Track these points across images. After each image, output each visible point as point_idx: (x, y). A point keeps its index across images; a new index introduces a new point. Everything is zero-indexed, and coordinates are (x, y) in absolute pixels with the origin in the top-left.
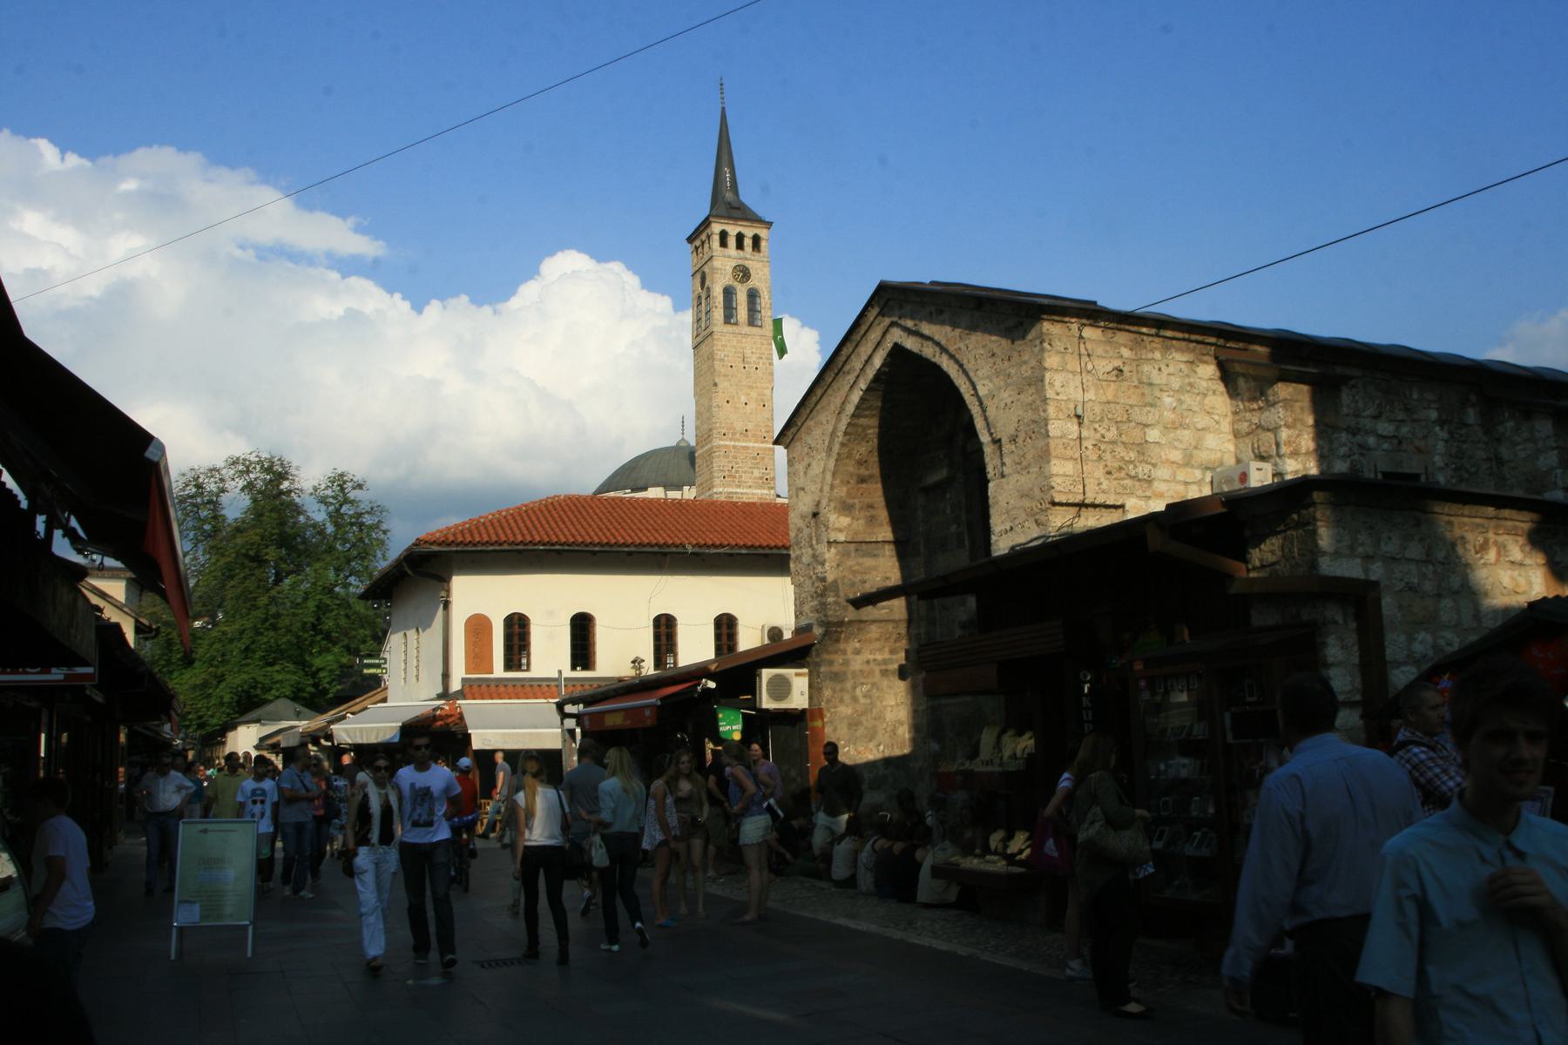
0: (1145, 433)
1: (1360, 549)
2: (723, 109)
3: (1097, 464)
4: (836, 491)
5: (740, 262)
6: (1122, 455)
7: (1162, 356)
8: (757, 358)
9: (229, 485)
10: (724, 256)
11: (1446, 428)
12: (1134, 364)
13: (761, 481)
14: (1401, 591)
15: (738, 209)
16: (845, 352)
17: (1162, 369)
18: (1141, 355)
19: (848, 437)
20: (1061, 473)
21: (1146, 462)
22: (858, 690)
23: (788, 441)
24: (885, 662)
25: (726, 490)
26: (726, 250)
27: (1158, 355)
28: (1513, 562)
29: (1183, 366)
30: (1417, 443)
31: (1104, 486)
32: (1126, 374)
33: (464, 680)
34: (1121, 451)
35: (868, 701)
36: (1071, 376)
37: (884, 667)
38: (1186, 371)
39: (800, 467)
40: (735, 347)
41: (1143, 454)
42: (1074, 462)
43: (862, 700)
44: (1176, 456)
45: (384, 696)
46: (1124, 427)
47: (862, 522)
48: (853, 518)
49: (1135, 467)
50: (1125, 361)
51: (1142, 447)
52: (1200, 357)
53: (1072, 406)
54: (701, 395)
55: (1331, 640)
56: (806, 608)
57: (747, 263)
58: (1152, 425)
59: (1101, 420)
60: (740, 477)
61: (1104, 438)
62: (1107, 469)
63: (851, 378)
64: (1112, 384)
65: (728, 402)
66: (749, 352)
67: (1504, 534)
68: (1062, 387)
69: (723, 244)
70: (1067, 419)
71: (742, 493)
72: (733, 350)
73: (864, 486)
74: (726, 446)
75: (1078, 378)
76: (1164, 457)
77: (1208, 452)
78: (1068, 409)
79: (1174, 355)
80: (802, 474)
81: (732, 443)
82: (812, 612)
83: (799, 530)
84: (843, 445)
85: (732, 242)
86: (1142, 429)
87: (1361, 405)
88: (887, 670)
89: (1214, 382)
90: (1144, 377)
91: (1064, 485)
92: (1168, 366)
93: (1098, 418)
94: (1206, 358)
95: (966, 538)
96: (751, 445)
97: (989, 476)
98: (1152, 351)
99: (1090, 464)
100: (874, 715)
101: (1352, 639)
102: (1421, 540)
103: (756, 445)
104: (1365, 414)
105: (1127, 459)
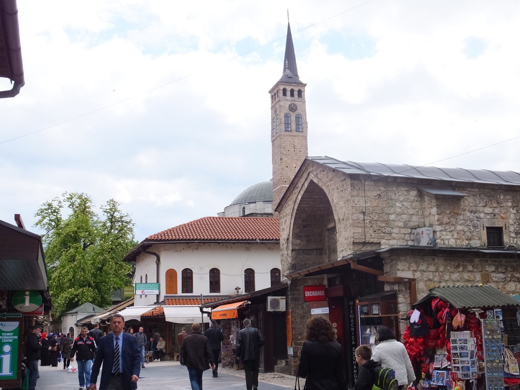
0: (389, 217)
1: (412, 268)
3: (370, 228)
5: (292, 102)
6: (380, 225)
7: (396, 189)
8: (300, 146)
9: (63, 204)
10: (285, 100)
11: (515, 209)
12: (385, 193)
14: (426, 281)
16: (296, 180)
21: (389, 227)
22: (304, 305)
26: (286, 97)
27: (395, 189)
28: (469, 271)
29: (405, 192)
30: (502, 215)
32: (382, 196)
33: (165, 297)
34: (379, 223)
36: (361, 198)
38: (406, 194)
40: (290, 142)
41: (388, 224)
43: (306, 308)
44: (401, 224)
45: (133, 302)
46: (381, 215)
48: (301, 240)
49: (385, 229)
50: (382, 191)
51: (387, 222)
52: (411, 188)
53: (361, 208)
54: (275, 163)
55: (400, 296)
57: (296, 103)
59: (372, 213)
61: (373, 219)
65: (287, 167)
66: (296, 143)
67: (466, 262)
69: (285, 94)
72: (289, 143)
73: (305, 228)
75: (364, 199)
78: (360, 210)
79: (401, 188)
80: (284, 223)
84: (296, 214)
85: (288, 93)
86: (388, 215)
87: (478, 202)
98: (393, 187)
99: (368, 228)
101: (407, 296)
102: (434, 265)
104: (479, 205)
105: (382, 226)
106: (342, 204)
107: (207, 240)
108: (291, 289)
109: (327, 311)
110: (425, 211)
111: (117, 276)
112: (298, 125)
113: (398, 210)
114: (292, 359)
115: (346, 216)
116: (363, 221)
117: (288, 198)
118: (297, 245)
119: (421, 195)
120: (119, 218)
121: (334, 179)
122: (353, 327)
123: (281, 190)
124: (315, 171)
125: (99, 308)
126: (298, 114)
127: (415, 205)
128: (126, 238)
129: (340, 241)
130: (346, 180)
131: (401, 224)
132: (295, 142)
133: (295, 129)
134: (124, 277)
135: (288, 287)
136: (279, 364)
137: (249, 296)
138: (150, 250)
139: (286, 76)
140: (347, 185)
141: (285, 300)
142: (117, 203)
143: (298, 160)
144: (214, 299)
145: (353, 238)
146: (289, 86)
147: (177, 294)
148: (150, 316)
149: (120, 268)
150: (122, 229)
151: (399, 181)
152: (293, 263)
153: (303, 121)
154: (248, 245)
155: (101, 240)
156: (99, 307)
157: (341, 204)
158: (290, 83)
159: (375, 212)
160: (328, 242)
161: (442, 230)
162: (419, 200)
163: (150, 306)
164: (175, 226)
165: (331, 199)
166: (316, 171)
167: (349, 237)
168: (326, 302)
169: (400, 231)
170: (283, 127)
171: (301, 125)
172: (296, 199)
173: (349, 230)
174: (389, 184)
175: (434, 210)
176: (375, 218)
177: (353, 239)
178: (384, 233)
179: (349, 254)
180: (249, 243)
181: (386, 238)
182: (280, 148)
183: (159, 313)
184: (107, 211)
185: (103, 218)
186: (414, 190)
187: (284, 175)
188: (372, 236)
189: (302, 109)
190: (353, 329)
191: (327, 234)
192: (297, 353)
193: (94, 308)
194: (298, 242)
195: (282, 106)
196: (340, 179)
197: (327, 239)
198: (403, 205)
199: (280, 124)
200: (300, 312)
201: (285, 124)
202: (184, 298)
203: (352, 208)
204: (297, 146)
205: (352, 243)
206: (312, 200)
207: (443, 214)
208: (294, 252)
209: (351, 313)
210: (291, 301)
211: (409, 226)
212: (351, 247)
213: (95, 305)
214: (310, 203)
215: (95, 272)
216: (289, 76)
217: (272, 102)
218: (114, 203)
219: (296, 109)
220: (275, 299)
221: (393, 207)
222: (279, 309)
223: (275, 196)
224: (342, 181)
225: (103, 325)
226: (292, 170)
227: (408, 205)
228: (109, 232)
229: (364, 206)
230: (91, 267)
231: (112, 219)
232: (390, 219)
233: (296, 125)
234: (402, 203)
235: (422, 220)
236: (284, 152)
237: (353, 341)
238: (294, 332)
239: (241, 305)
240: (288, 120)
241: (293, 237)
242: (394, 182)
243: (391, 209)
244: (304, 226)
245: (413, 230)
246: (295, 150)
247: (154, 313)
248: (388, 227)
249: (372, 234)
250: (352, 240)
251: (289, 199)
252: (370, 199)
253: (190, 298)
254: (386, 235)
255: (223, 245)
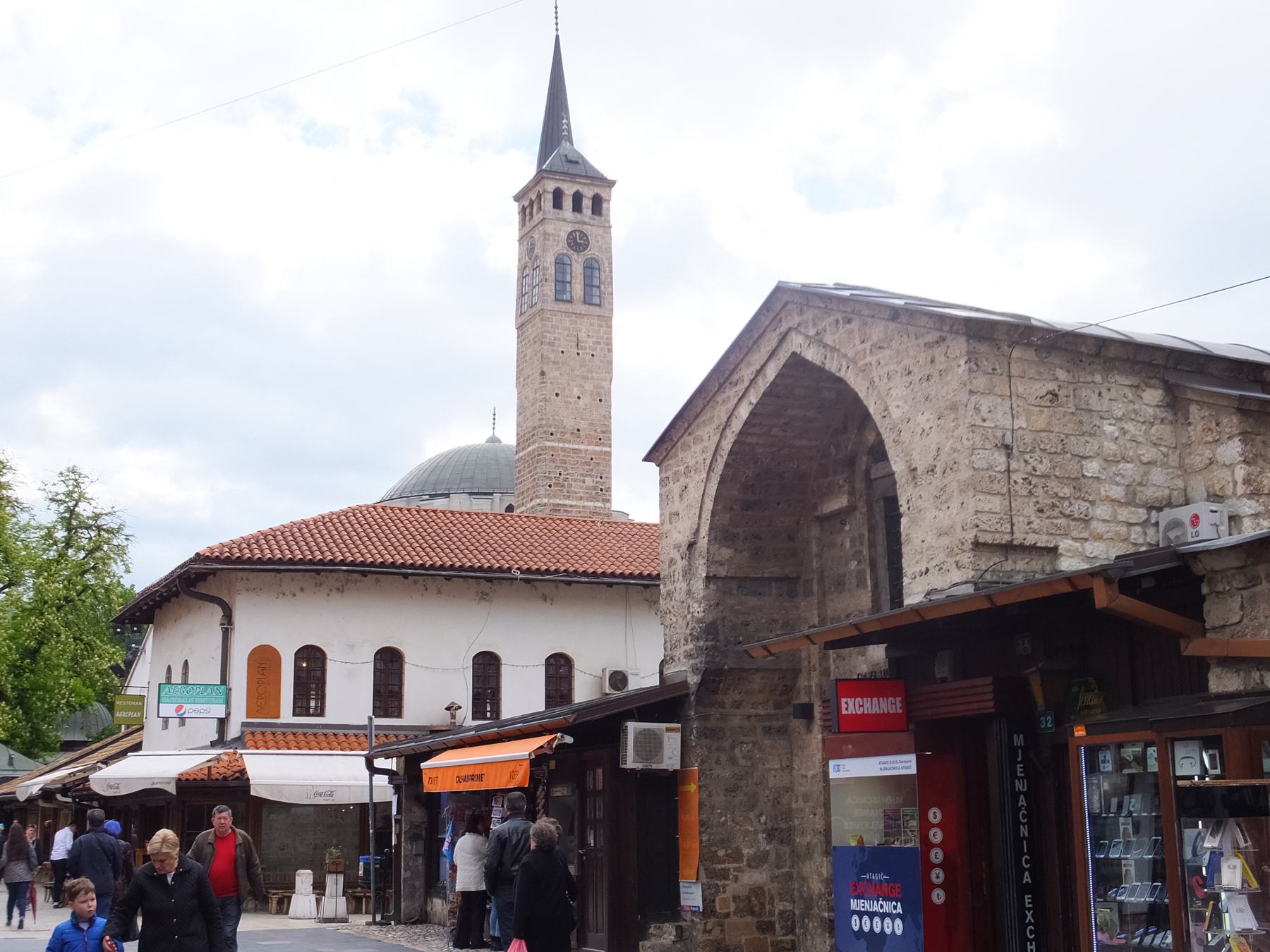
0: (1082, 466)
2: (557, 37)
3: (1027, 500)
4: (717, 518)
5: (577, 227)
6: (1055, 490)
7: (1103, 378)
10: (558, 219)
12: (1071, 388)
13: (594, 492)
15: (577, 163)
17: (1103, 394)
18: (1079, 377)
19: (733, 457)
20: (986, 509)
21: (1083, 499)
22: (737, 751)
23: (661, 458)
24: (768, 717)
25: (551, 501)
29: (1127, 390)
31: (1034, 526)
32: (1062, 399)
33: (244, 724)
34: (1053, 485)
35: (749, 763)
36: (999, 400)
37: (768, 724)
38: (1130, 396)
39: (675, 488)
40: (568, 329)
41: (1080, 490)
42: (1002, 498)
43: (742, 762)
44: (1118, 492)
45: (138, 740)
46: (1059, 459)
47: (745, 554)
48: (736, 550)
49: (1071, 504)
50: (1061, 384)
51: (1078, 482)
52: (1146, 380)
53: (999, 434)
54: (524, 385)
56: (679, 653)
57: (586, 229)
58: (1090, 457)
59: (1032, 451)
60: (570, 486)
61: (1035, 470)
62: (1038, 506)
63: (741, 387)
64: (1046, 409)
65: (557, 395)
68: (990, 412)
69: (558, 204)
70: (995, 449)
71: (571, 506)
72: (566, 332)
74: (553, 448)
75: (1007, 403)
76: (1103, 493)
77: (1154, 489)
78: (996, 437)
79: (1118, 378)
80: (677, 496)
81: (561, 445)
82: (685, 657)
83: (672, 560)
84: (727, 465)
85: (568, 203)
88: (770, 728)
89: (1162, 409)
90: (1082, 402)
91: (989, 523)
92: (1109, 390)
93: (1030, 448)
94: (1153, 382)
95: (868, 577)
96: (583, 447)
97: (902, 510)
98: (1092, 373)
99: (1019, 499)
100: (755, 780)
103: (590, 448)
105: (1062, 495)
106: (928, 420)
107: (372, 564)
108: (699, 701)
109: (909, 768)
110: (1190, 454)
111: (79, 674)
112: (588, 285)
113: (1110, 447)
114: (697, 920)
115: (943, 457)
116: (1006, 473)
117: (697, 416)
118: (721, 564)
119: (1175, 403)
120: (88, 518)
121: (893, 344)
122: (1024, 824)
123: (539, 455)
124: (811, 325)
125: (24, 757)
126: (591, 259)
127: (1158, 435)
128: (106, 571)
129: (916, 542)
130: (948, 342)
131: (1118, 492)
132: (580, 330)
133: (582, 297)
134: (97, 676)
135: (687, 695)
136: (655, 935)
137: (571, 720)
138: (203, 588)
139: (563, 158)
140: (951, 357)
141: (678, 736)
142: (86, 477)
143: (587, 378)
144: (386, 736)
145: (975, 530)
146: (570, 184)
147: (278, 717)
148: (202, 780)
149: (85, 653)
150: (99, 548)
151: (1111, 352)
152: (710, 618)
153: (603, 279)
154: (485, 586)
155: (38, 576)
156: (24, 754)
157: (925, 419)
158: (573, 174)
159: (1041, 449)
160: (820, 556)
161: (1259, 513)
162: (1170, 417)
163: (203, 752)
164: (278, 525)
165: (875, 409)
166: (814, 325)
167: (959, 527)
168: (907, 738)
169: (1115, 514)
170: (549, 289)
171: (596, 286)
172: (729, 418)
173: (955, 504)
174: (1081, 361)
175: (1232, 450)
176: (1042, 469)
177: (974, 531)
178: (1069, 516)
179: (957, 580)
180: (489, 580)
181: (1075, 534)
182: (542, 343)
183: (229, 773)
184: (58, 497)
185: (48, 515)
186: (1152, 387)
187: (549, 416)
188: (1032, 526)
189: (600, 247)
190: (1024, 831)
191: (815, 531)
192: (714, 901)
193: (11, 759)
194: (726, 553)
195: (549, 234)
196: (921, 341)
197: (814, 549)
198: (1124, 432)
199: (544, 283)
200: (725, 772)
201: (556, 281)
202: (300, 731)
203: (973, 432)
204: (586, 342)
205: (968, 546)
206: (782, 421)
207: (1261, 462)
208: (711, 586)
209: (1019, 774)
210: (698, 738)
211: (1140, 500)
212: (966, 558)
213: (14, 750)
214: (774, 431)
215: (18, 660)
216: (569, 158)
217: (523, 223)
218: (77, 477)
219: (586, 246)
220: (649, 730)
221: (1095, 435)
222: (661, 762)
223: (519, 472)
224: (928, 346)
225: (46, 805)
226: (570, 403)
227: (1139, 433)
228: (60, 555)
229: (1008, 425)
230: (8, 646)
231: (70, 518)
232: (1086, 474)
233: (585, 285)
234: (1120, 424)
235: (1180, 484)
236: (552, 356)
237: (1027, 873)
238: (705, 838)
239: (542, 747)
240: (564, 273)
241: (712, 537)
242: (1098, 355)
243: (1087, 442)
244: (747, 507)
245: (1154, 513)
246: (580, 352)
247: (214, 771)
248: (1078, 498)
249: (1032, 519)
250: (970, 536)
251: (701, 419)
252: (1026, 406)
253: (315, 731)
254: (1074, 523)
255: (415, 582)
